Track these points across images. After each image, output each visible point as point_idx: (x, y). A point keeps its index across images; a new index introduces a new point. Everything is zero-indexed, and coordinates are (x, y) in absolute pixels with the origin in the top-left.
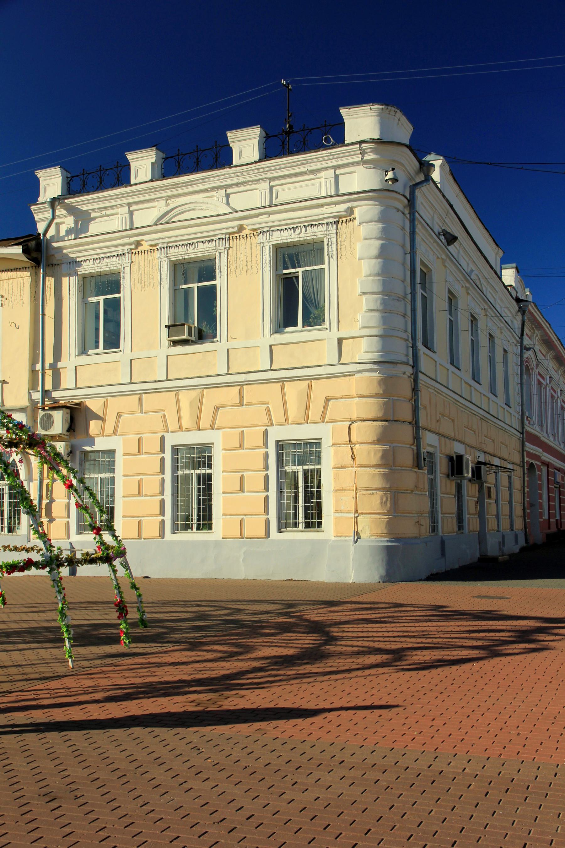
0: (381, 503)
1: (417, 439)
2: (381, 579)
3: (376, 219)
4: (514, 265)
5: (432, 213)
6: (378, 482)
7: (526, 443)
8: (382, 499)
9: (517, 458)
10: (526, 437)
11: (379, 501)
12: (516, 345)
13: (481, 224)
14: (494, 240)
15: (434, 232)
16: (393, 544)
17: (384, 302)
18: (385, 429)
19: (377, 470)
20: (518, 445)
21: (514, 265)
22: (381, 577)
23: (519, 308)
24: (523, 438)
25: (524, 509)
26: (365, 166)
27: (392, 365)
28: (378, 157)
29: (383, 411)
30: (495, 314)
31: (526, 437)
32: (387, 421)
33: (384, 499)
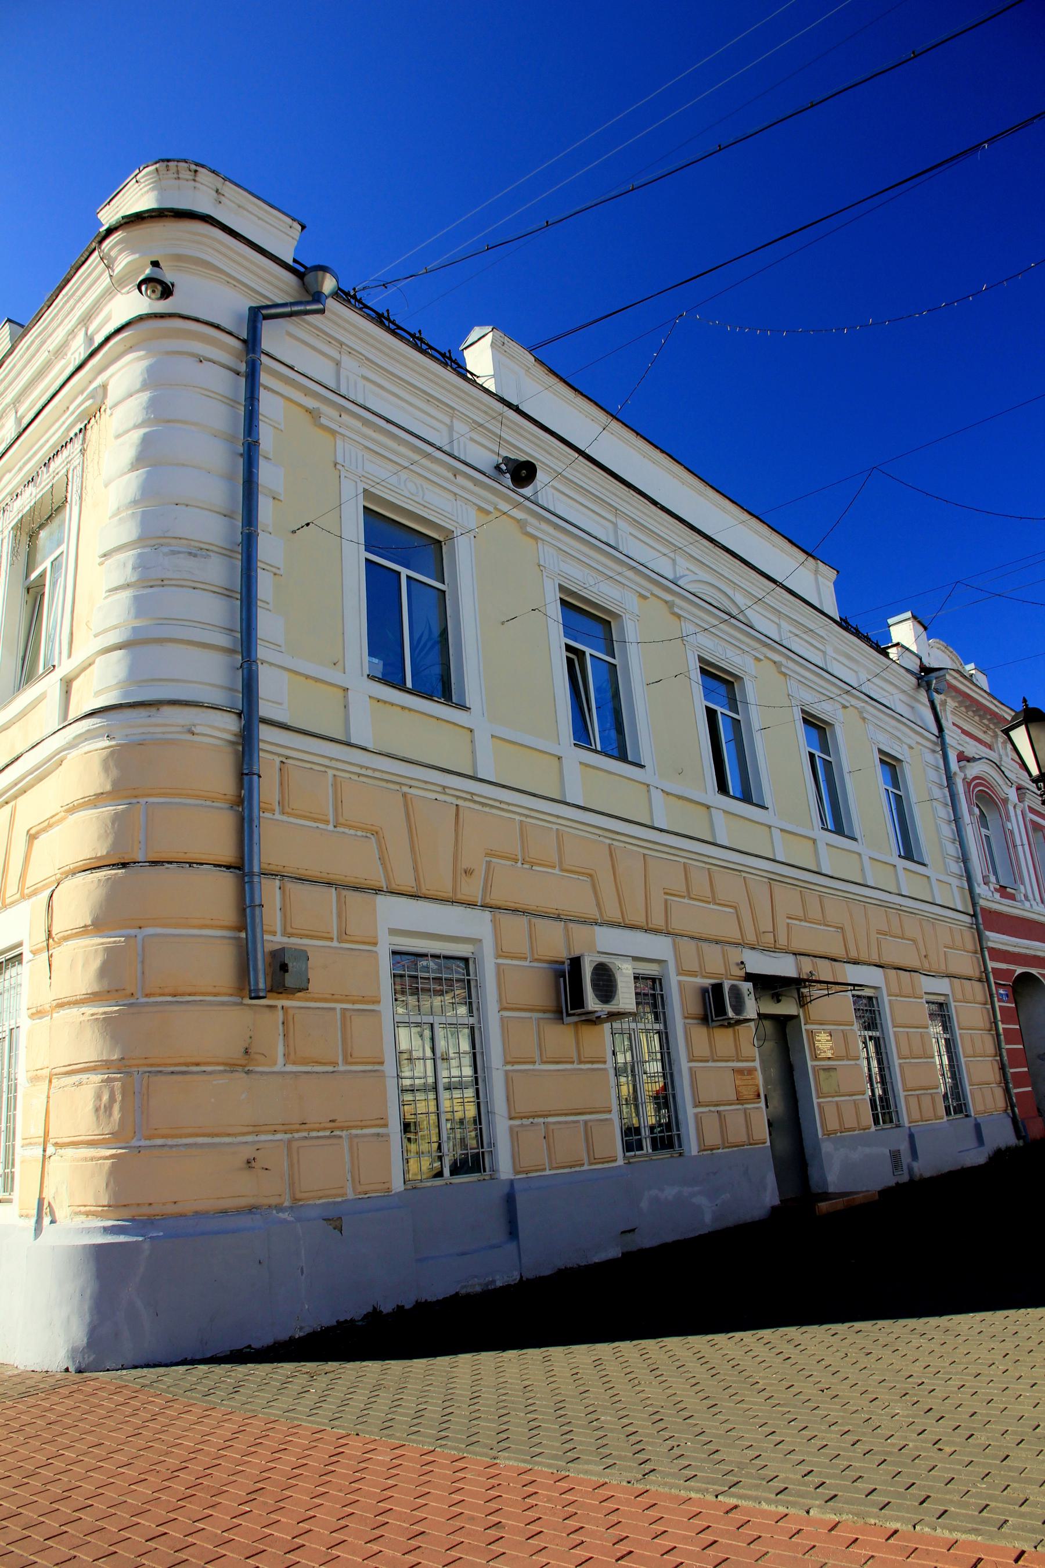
0: (97, 1110)
1: (246, 911)
2: (73, 1359)
3: (138, 386)
4: (909, 614)
5: (447, 420)
6: (91, 1048)
7: (987, 933)
8: (99, 1097)
9: (966, 963)
10: (985, 920)
11: (90, 1106)
12: (934, 751)
13: (727, 502)
14: (790, 541)
15: (982, 689)
16: (122, 1239)
17: (142, 565)
18: (113, 889)
19: (89, 1010)
20: (969, 940)
21: (909, 614)
22: (73, 1353)
23: (918, 679)
24: (977, 924)
25: (1002, 1068)
26: (124, 291)
27: (142, 712)
28: (137, 256)
29: (110, 840)
30: (840, 688)
31: (985, 920)
32: (124, 865)
33: (105, 1098)
